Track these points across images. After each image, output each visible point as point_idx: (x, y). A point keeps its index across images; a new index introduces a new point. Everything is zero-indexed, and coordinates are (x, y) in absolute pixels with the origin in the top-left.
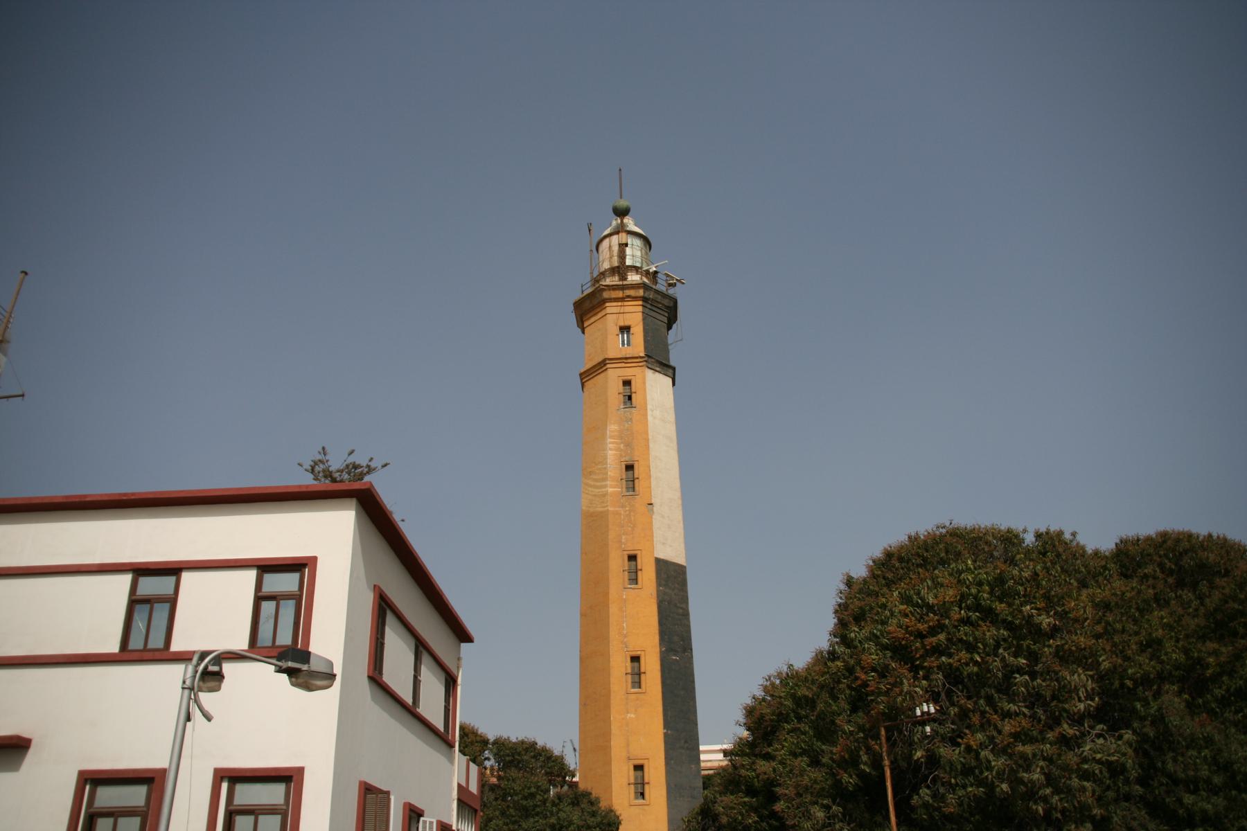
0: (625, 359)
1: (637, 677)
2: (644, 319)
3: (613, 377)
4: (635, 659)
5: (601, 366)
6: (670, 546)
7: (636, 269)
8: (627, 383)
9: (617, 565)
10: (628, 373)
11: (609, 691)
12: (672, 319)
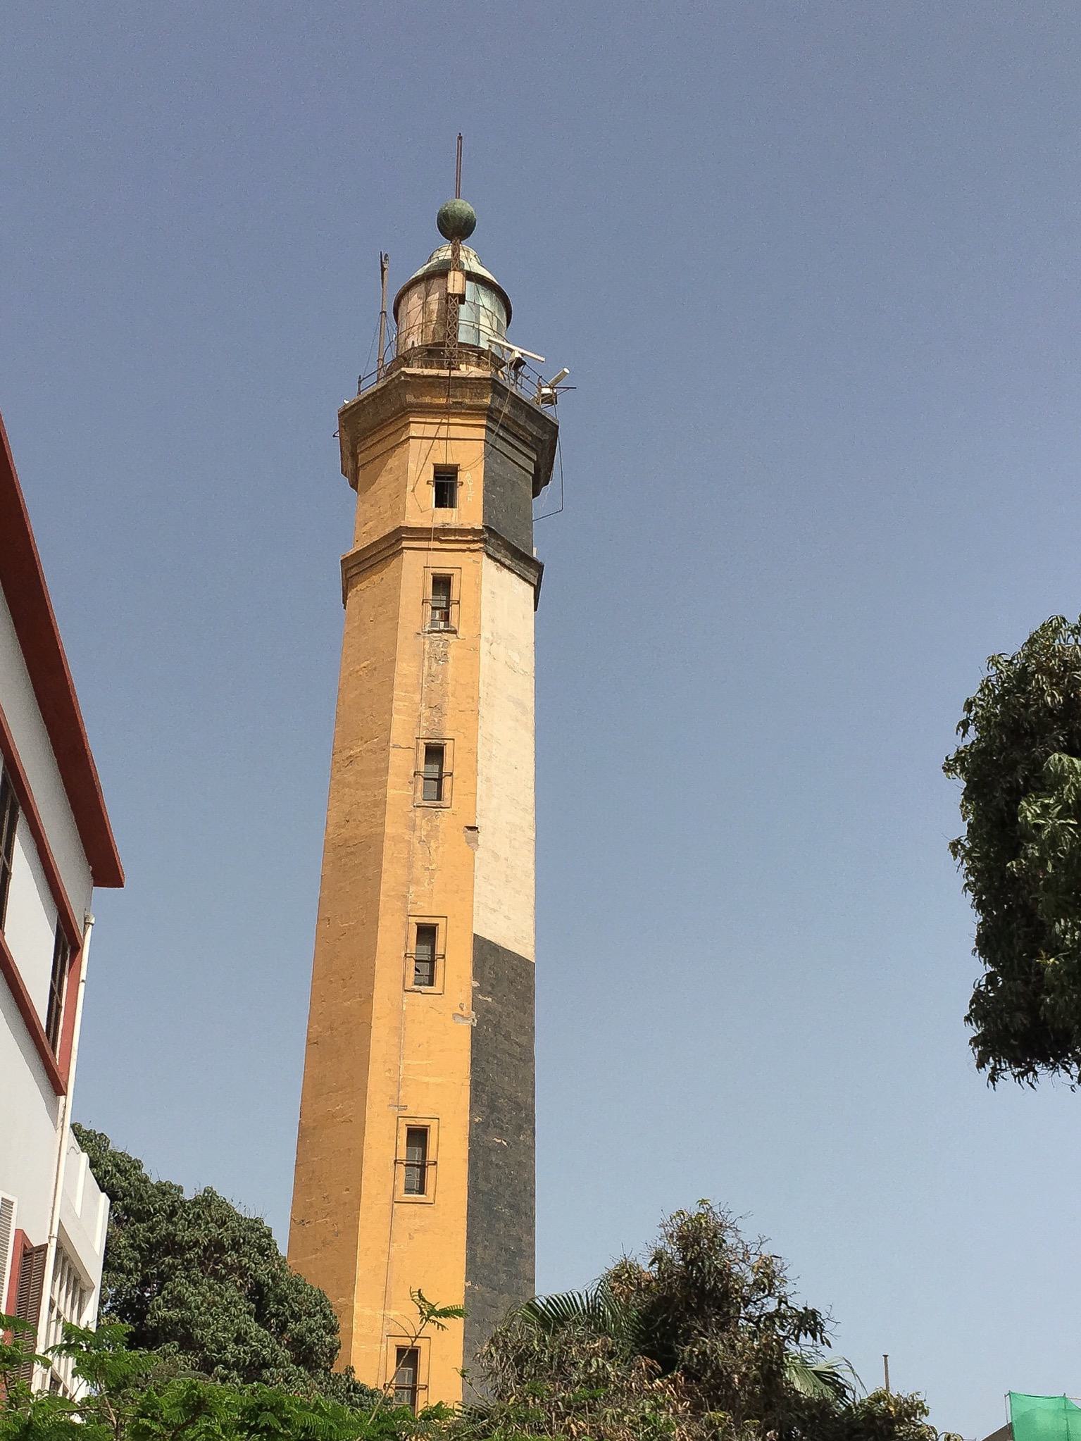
0: (442, 533)
1: (418, 1172)
2: (488, 455)
3: (415, 567)
4: (418, 1136)
5: (389, 547)
6: (504, 909)
7: (481, 355)
8: (442, 584)
9: (393, 942)
10: (444, 561)
11: (358, 1197)
12: (540, 478)
